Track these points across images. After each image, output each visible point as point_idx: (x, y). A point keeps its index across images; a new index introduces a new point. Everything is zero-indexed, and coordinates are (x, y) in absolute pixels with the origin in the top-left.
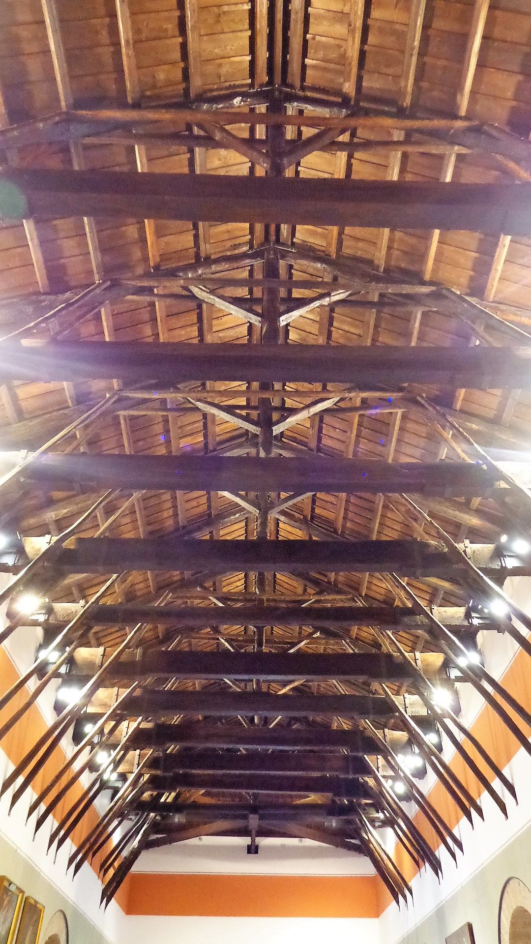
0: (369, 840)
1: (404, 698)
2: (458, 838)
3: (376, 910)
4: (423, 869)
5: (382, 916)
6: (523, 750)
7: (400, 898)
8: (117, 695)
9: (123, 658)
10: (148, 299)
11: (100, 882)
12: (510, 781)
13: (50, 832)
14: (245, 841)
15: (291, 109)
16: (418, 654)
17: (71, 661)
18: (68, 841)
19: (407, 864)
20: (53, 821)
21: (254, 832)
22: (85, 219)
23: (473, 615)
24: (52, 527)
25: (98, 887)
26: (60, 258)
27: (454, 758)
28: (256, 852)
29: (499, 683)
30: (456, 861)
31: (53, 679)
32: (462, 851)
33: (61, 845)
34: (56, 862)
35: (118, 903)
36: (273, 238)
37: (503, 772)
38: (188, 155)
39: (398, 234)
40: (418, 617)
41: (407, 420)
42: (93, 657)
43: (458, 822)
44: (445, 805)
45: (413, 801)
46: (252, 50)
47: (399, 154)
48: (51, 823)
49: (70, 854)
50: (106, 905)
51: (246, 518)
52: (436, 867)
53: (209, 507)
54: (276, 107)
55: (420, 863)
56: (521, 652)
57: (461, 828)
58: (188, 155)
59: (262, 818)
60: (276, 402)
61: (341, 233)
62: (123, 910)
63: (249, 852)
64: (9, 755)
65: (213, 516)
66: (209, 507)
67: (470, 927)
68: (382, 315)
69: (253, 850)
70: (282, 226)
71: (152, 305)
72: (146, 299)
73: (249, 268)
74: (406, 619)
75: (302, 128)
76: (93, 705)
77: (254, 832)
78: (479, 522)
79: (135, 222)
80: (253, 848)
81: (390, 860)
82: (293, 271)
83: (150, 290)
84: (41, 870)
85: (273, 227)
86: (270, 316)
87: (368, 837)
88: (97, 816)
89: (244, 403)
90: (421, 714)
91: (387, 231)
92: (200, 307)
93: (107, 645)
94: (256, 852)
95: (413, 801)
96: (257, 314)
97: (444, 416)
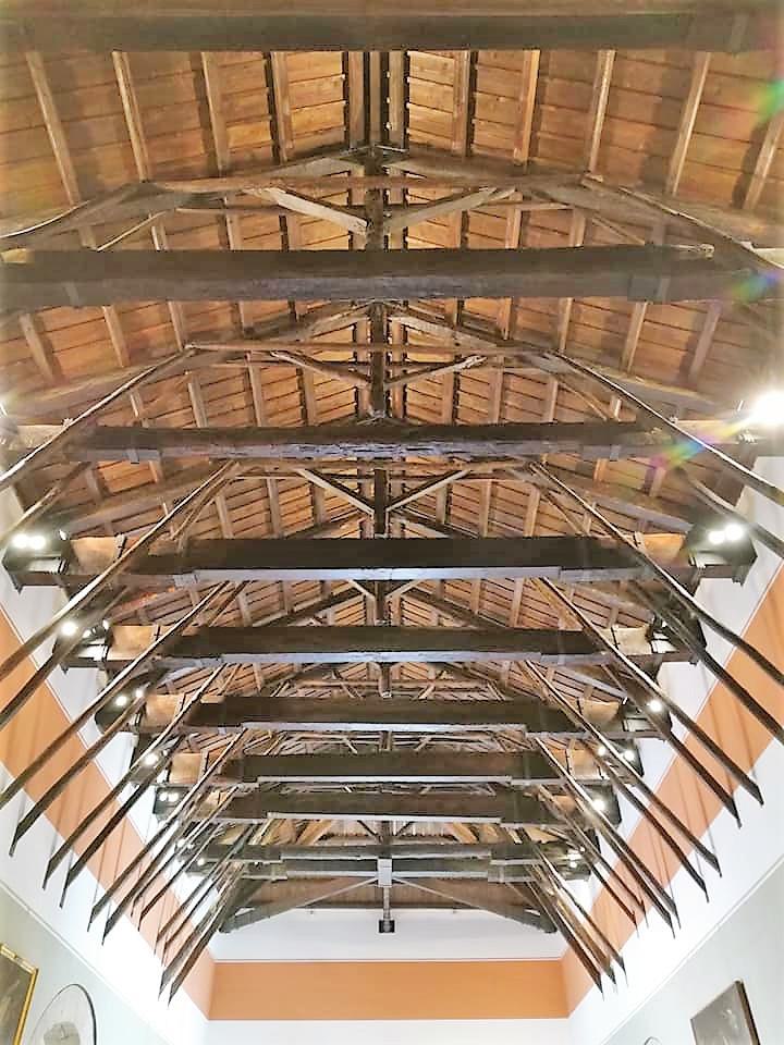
0: (555, 898)
1: (612, 631)
2: (709, 849)
3: (561, 1005)
4: (642, 925)
6: (775, 741)
7: (604, 977)
8: (123, 547)
9: (155, 549)
10: (218, 212)
11: (157, 960)
13: (49, 852)
16: (638, 535)
17: (67, 553)
18: (86, 875)
21: (387, 903)
23: (657, 636)
24: (110, 530)
25: (153, 965)
26: (141, 329)
27: (638, 830)
28: (392, 930)
31: (119, 734)
35: (187, 992)
36: (375, 138)
38: (264, 61)
39: (555, 55)
40: (647, 434)
42: (107, 550)
44: (687, 797)
45: (559, 932)
49: (54, 848)
50: (173, 993)
52: (668, 909)
53: (305, 414)
54: (376, 171)
56: (568, 950)
57: (719, 831)
58: (264, 61)
59: (397, 866)
60: (395, 357)
63: (381, 930)
64: (7, 765)
66: (305, 414)
67: (740, 987)
68: (539, 134)
69: (387, 926)
71: (247, 373)
72: (236, 366)
75: (409, 53)
77: (387, 903)
79: (242, 389)
80: (387, 923)
82: (408, 105)
83: (239, 356)
84: (29, 909)
85: (375, 56)
86: (375, 225)
87: (554, 890)
88: (60, 713)
91: (537, 53)
94: (392, 930)
95: (559, 932)
96: (364, 378)
97: (584, 473)
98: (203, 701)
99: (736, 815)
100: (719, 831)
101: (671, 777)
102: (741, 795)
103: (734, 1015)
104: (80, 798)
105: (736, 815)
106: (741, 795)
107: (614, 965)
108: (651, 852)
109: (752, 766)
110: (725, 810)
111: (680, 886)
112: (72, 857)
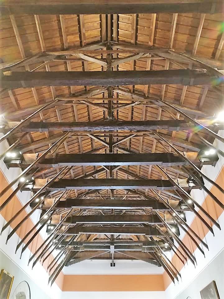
3: (163, 287)
4: (186, 264)
5: (166, 290)
7: (175, 279)
11: (48, 274)
12: (206, 243)
14: (110, 261)
15: (115, 48)
18: (27, 249)
19: (178, 263)
20: (19, 238)
22: (35, 15)
23: (190, 182)
25: (46, 275)
28: (114, 266)
29: (214, 182)
30: (204, 254)
32: (208, 248)
33: (24, 251)
34: (21, 258)
36: (109, 39)
37: (203, 240)
39: (161, 15)
40: (187, 123)
41: (178, 34)
42: (33, 157)
43: (205, 236)
44: (199, 228)
46: (101, 27)
47: (150, 60)
48: (16, 239)
51: (103, 92)
52: (193, 260)
55: (184, 262)
57: (208, 238)
61: (137, 16)
62: (57, 285)
65: (87, 91)
67: (214, 282)
70: (114, 15)
72: (69, 105)
73: (103, 93)
74: (182, 124)
75: (119, 15)
76: (36, 186)
78: (220, 64)
80: (113, 264)
81: (170, 261)
83: (71, 102)
87: (161, 255)
89: (104, 135)
90: (186, 186)
92: (83, 63)
93: (56, 197)
94: (114, 266)
97: (169, 135)
98: (60, 200)
99: (213, 233)
100: (208, 238)
101: (194, 222)
102: (214, 227)
103: (213, 290)
104: (25, 228)
105: (213, 233)
106: (214, 227)
107: (178, 276)
108: (189, 243)
109: (217, 219)
110: (210, 232)
111: (197, 253)
112: (24, 245)
